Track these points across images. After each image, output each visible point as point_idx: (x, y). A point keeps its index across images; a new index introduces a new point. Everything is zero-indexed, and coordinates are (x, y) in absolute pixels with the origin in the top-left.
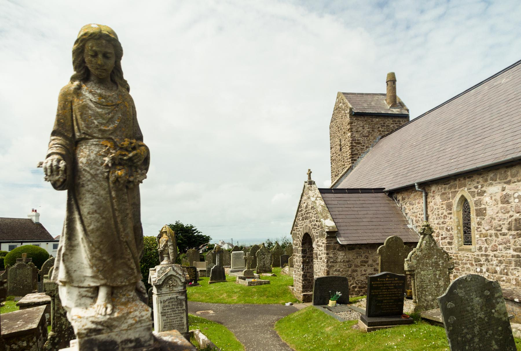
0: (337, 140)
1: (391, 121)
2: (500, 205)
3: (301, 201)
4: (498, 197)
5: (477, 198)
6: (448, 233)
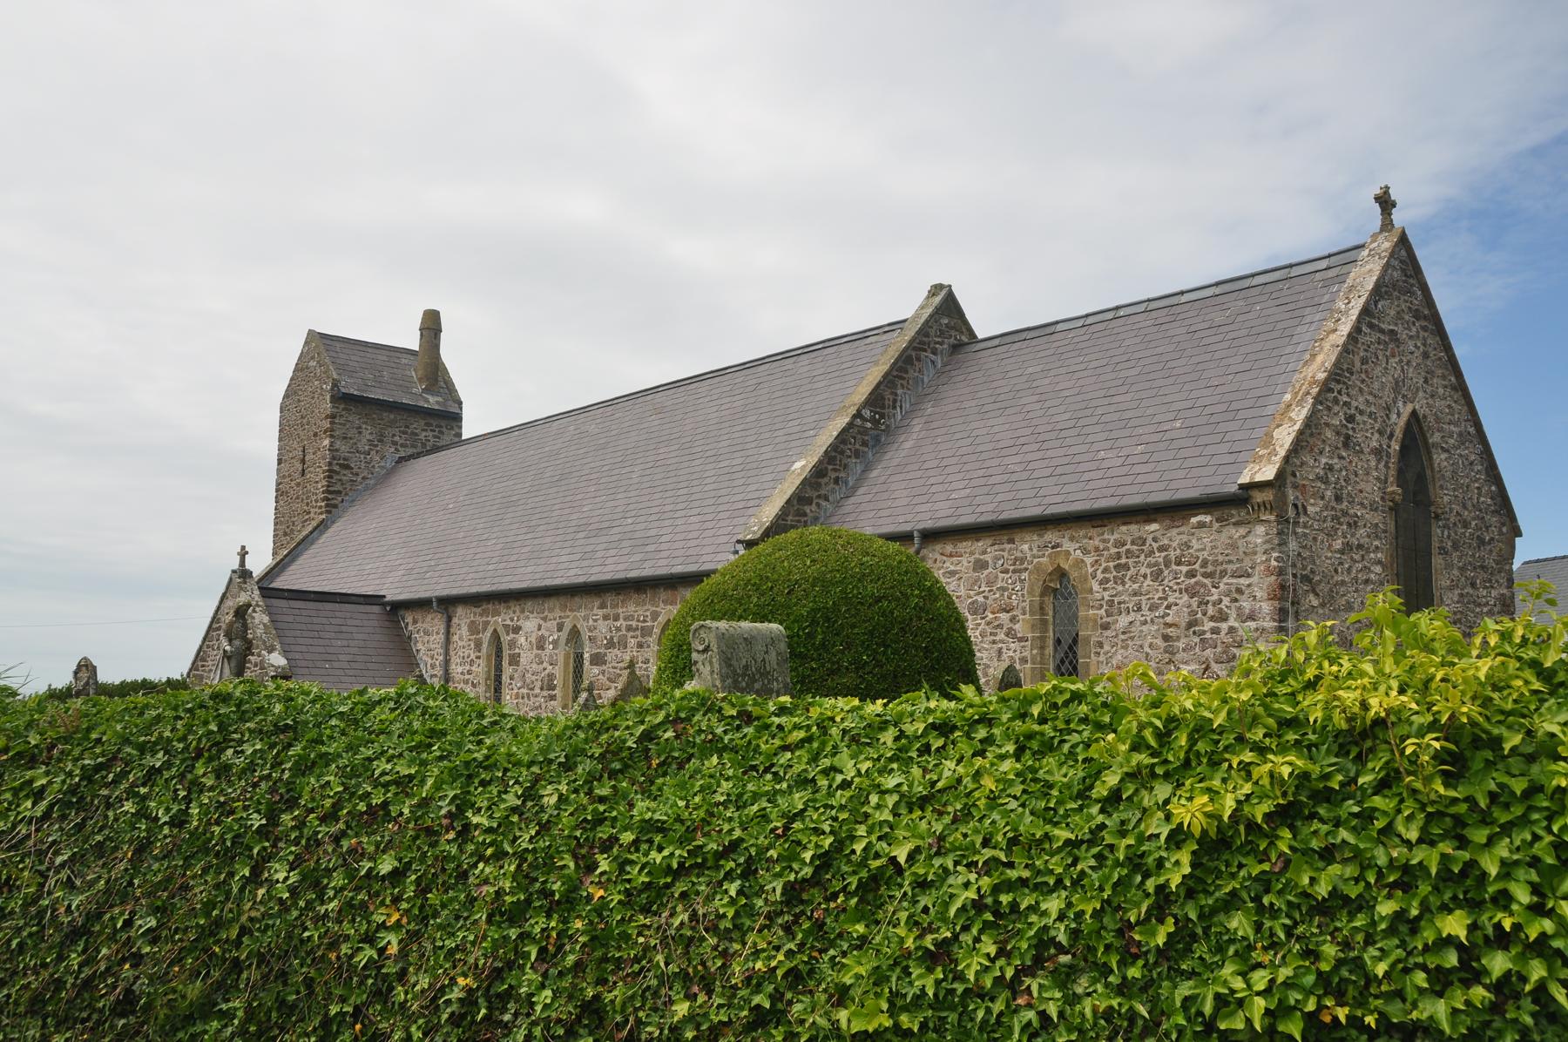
0: (295, 445)
3: (218, 608)
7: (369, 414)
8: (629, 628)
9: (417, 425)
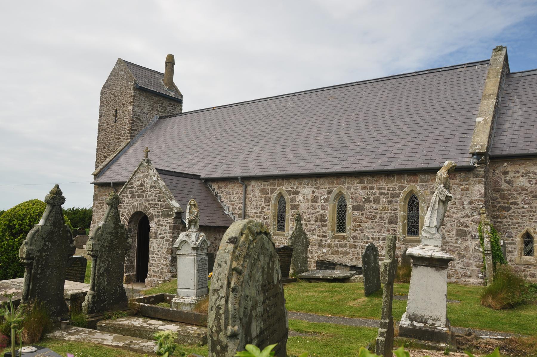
1: (168, 103)
2: (310, 203)
4: (309, 198)
5: (292, 196)
6: (265, 221)
7: (144, 97)
8: (381, 194)
9: (166, 103)
